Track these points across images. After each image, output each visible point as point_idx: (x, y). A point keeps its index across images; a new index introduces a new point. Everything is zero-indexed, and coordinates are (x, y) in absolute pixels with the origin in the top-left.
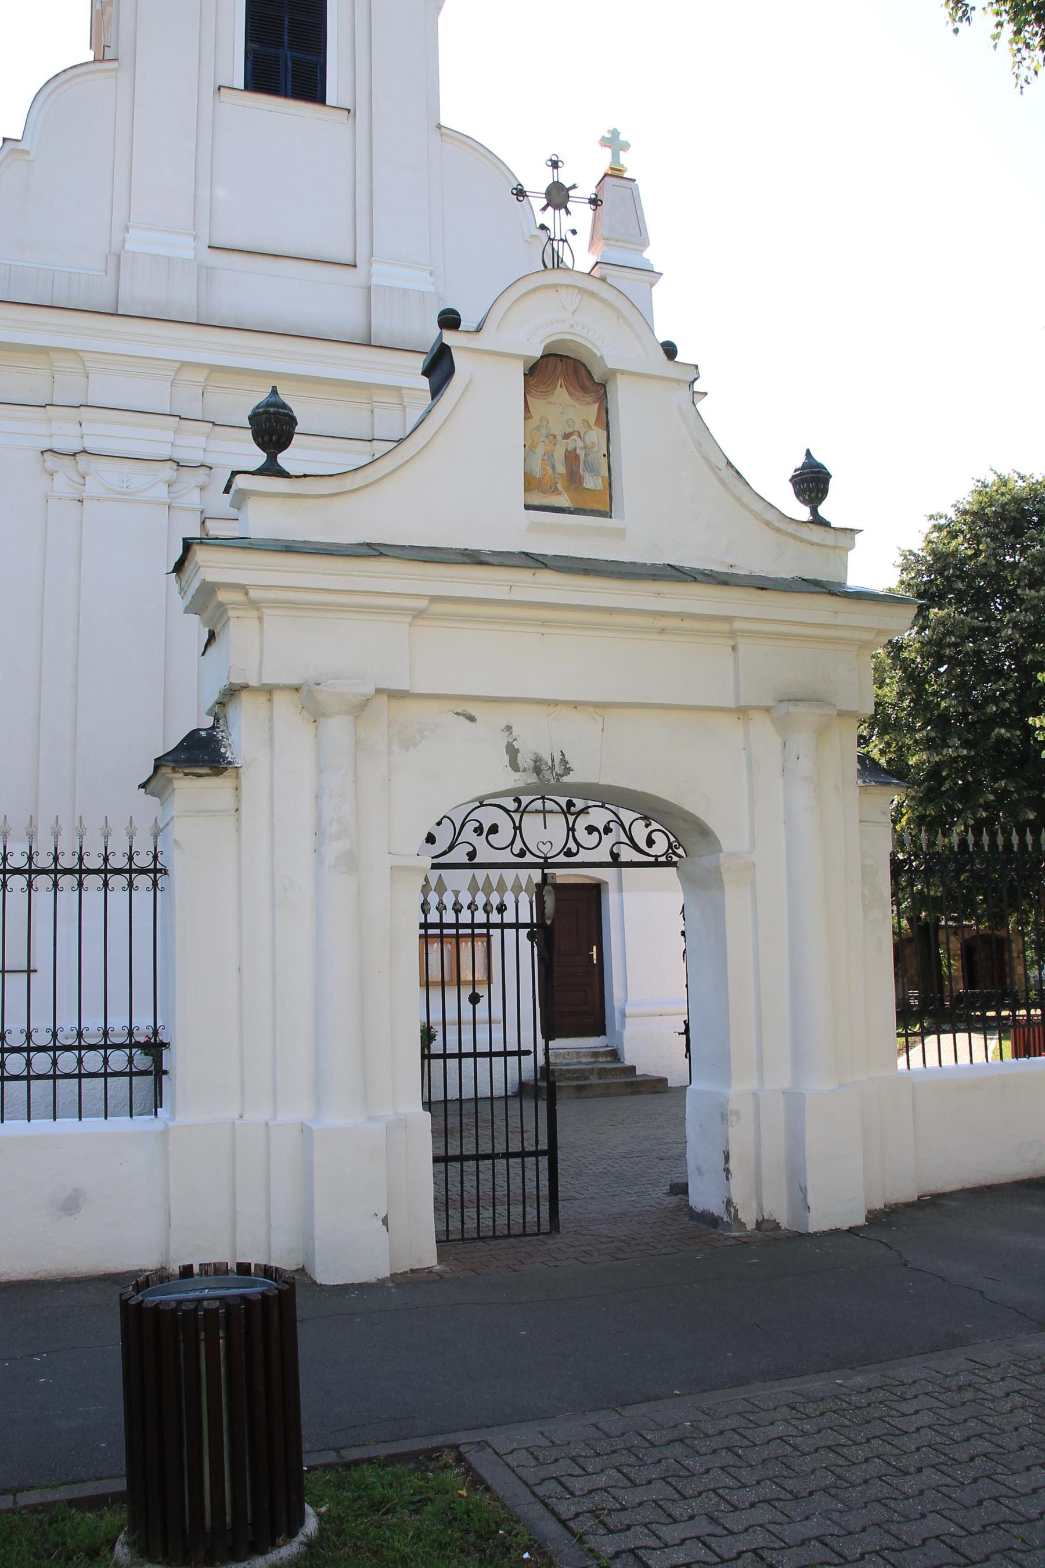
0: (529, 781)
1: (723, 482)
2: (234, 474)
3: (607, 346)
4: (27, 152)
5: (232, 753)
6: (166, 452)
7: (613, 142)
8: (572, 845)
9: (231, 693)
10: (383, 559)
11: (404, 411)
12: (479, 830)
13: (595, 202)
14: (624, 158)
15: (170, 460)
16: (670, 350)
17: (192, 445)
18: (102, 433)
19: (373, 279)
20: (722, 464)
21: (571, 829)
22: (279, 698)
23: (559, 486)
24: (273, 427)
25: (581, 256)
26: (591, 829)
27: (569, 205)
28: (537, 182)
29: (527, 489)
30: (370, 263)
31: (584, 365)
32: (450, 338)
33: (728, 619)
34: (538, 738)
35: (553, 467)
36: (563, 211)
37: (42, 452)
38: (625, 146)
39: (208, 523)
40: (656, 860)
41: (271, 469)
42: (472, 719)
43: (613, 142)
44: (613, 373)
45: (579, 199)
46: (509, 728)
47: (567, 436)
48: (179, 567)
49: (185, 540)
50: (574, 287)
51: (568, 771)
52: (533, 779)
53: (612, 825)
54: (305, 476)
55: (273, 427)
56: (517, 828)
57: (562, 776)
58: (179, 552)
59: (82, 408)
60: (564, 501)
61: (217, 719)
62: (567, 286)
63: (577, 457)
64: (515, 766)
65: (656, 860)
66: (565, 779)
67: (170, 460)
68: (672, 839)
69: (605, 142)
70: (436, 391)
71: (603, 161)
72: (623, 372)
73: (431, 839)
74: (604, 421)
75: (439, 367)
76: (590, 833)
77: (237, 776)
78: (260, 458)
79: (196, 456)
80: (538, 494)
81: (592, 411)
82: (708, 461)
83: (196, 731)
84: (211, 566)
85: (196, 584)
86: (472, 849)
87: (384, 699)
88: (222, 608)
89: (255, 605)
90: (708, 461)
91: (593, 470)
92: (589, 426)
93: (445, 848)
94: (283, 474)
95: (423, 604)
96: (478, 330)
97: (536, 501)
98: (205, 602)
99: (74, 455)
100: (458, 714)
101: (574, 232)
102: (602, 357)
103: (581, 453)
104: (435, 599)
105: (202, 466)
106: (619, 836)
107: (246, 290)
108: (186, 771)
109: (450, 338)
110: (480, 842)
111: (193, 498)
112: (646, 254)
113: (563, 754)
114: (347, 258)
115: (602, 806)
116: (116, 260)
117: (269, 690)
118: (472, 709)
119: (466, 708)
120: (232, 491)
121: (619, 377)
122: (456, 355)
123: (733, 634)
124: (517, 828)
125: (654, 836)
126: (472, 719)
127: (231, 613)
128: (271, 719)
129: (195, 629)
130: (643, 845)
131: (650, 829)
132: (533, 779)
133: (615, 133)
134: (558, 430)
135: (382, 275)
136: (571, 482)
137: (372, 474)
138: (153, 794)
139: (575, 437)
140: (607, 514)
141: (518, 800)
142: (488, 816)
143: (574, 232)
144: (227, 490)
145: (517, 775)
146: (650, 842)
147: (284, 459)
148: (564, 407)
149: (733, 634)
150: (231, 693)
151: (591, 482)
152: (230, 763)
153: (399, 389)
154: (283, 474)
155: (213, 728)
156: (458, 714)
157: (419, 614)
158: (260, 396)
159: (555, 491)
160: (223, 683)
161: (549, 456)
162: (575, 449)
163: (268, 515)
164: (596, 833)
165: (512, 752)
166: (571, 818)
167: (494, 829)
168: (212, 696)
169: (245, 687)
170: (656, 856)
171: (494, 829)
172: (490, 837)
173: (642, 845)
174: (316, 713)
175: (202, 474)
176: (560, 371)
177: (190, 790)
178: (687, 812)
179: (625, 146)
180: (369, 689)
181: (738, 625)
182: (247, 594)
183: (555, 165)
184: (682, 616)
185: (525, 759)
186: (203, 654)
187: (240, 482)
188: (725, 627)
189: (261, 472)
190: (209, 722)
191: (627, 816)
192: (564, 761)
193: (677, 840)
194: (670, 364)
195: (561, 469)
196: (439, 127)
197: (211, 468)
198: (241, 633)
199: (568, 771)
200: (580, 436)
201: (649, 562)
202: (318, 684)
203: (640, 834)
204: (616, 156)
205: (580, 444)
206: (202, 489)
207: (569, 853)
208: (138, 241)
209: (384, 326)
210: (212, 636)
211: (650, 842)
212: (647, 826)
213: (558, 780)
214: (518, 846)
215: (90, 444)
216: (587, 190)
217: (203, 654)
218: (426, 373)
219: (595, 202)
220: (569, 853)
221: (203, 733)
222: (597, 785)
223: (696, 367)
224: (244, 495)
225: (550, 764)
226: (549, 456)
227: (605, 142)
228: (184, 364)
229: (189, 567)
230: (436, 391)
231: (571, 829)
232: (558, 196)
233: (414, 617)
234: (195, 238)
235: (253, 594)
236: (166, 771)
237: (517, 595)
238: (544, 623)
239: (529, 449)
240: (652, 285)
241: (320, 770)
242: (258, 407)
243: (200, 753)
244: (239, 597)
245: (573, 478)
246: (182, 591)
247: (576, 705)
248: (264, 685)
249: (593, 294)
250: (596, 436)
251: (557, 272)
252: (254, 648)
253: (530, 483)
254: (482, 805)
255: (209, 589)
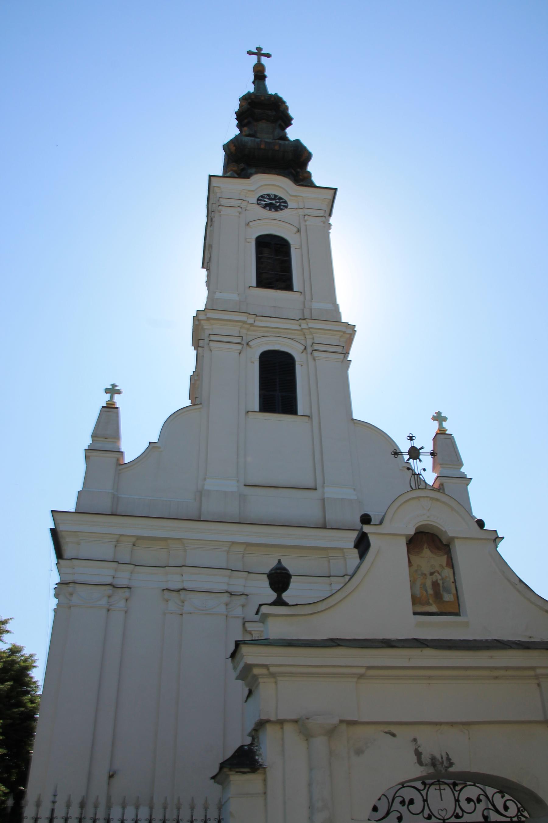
0: (430, 772)
1: (518, 591)
2: (261, 605)
3: (447, 524)
4: (159, 448)
5: (262, 759)
6: (225, 588)
7: (439, 418)
8: (458, 811)
9: (261, 725)
10: (340, 648)
11: (345, 560)
12: (403, 803)
13: (433, 454)
14: (445, 425)
15: (227, 592)
16: (481, 523)
17: (238, 583)
18: (192, 579)
19: (268, 82)
20: (517, 582)
21: (457, 801)
22: (288, 727)
23: (431, 601)
24: (280, 579)
25: (430, 477)
26: (469, 800)
27: (421, 457)
28: (404, 447)
29: (414, 603)
30: (323, 487)
31: (437, 536)
32: (367, 529)
33: (533, 668)
34: (433, 744)
35: (426, 591)
36: (418, 460)
37: (163, 590)
38: (445, 419)
39: (247, 625)
40: (511, 820)
41: (279, 602)
42: (394, 735)
43: (439, 418)
44: (453, 539)
45: (425, 454)
46: (415, 740)
47: (432, 574)
48: (233, 655)
49: (236, 642)
50: (427, 497)
51: (451, 764)
52: (431, 770)
53: (482, 797)
54: (297, 605)
55: (280, 579)
56: (425, 801)
57: (448, 767)
58: (232, 648)
59: (183, 568)
60: (433, 608)
61: (253, 739)
62: (424, 497)
63: (438, 584)
64: (420, 763)
65: (511, 820)
66: (451, 770)
67: (227, 592)
68: (519, 805)
69: (434, 418)
70: (362, 555)
71: (435, 427)
72: (457, 538)
73: (375, 809)
74: (451, 564)
75: (362, 544)
76: (469, 803)
77: (265, 773)
78: (273, 596)
79: (240, 589)
80: (420, 605)
81: (443, 559)
82: (509, 581)
83: (241, 747)
84: (251, 655)
85: (241, 665)
86: (399, 815)
87: (344, 727)
88: (255, 678)
89: (273, 675)
90: (509, 581)
91: (448, 591)
92: (443, 567)
93: (383, 814)
94: (285, 604)
95: (362, 671)
96: (381, 523)
97: (419, 609)
98: (247, 674)
99: (179, 591)
100: (386, 733)
101: (424, 470)
102: (446, 532)
103: (440, 582)
104: (369, 668)
105: (243, 594)
106: (487, 805)
107: (263, 504)
108: (237, 770)
109: (367, 529)
110: (403, 810)
111: (238, 611)
112: (462, 470)
113: (447, 754)
114: (312, 485)
115: (474, 785)
116: (201, 494)
117: (281, 723)
118: (393, 729)
119: (390, 728)
120: (260, 613)
121: (456, 541)
122: (371, 538)
123: (537, 677)
124: (425, 801)
125: (508, 803)
126: (394, 735)
127: (260, 680)
128: (283, 739)
129: (241, 688)
130: (502, 810)
131: (505, 799)
132: (431, 770)
133: (439, 413)
134: (427, 571)
135: (330, 492)
136: (437, 597)
137: (331, 601)
138: (218, 783)
139: (436, 574)
140: (457, 614)
141: (424, 783)
142: (408, 794)
143: (424, 470)
144: (257, 613)
145: (422, 768)
146: (506, 808)
147: (285, 596)
148: (429, 559)
149: (537, 677)
150: (261, 725)
151: (447, 597)
152: (261, 765)
153: (342, 549)
154: (285, 604)
155: (252, 744)
156: (386, 733)
157: (361, 676)
158: (273, 564)
159: (428, 604)
160: (257, 719)
161: (424, 586)
162: (437, 581)
163: (278, 627)
164: (472, 803)
165: (418, 754)
166: (456, 793)
167: (411, 802)
168: (250, 726)
169: (268, 721)
170: (511, 818)
171: (411, 802)
172: (410, 806)
173: (501, 809)
174: (307, 734)
175: (242, 599)
176: (425, 540)
177: (239, 781)
178: (526, 788)
179: (445, 419)
180: (336, 721)
181: (539, 671)
182: (268, 669)
183: (411, 438)
184: (507, 668)
185: (426, 758)
186: (246, 701)
187: (264, 609)
188: (532, 673)
189: (274, 603)
190: (248, 741)
191: (490, 791)
192: (448, 759)
193: (522, 807)
194: (482, 531)
195: (430, 591)
196: (353, 420)
197: (247, 595)
198: (266, 689)
199: (451, 764)
200: (439, 573)
201: (484, 638)
202: (308, 719)
203: (499, 802)
204: (441, 424)
205: (439, 577)
206: (243, 606)
207: (457, 816)
208: (210, 485)
209: (332, 517)
210: (250, 692)
211: (506, 808)
212: (503, 797)
213: (446, 770)
214: (427, 812)
215: (186, 585)
216: (429, 447)
217: (246, 701)
218: (356, 546)
219: (433, 454)
220: (457, 816)
221: (246, 747)
222: (469, 773)
223: (496, 531)
224: (265, 616)
225: (440, 760)
226: (424, 586)
227: (434, 418)
228: (233, 543)
229: (238, 656)
230: (362, 555)
231: (457, 801)
232: (415, 453)
233: (359, 678)
234: (238, 481)
235: (272, 669)
236: (226, 770)
237: (413, 663)
238: (430, 677)
239: (413, 583)
240: (468, 485)
241: (311, 769)
242: (272, 570)
243: (245, 760)
244: (264, 671)
245: (438, 596)
246: (235, 668)
247: (452, 724)
248: (279, 720)
249: (437, 500)
250: (447, 572)
251: (419, 491)
252: (275, 700)
253: (415, 600)
254: (403, 787)
255: (248, 668)
